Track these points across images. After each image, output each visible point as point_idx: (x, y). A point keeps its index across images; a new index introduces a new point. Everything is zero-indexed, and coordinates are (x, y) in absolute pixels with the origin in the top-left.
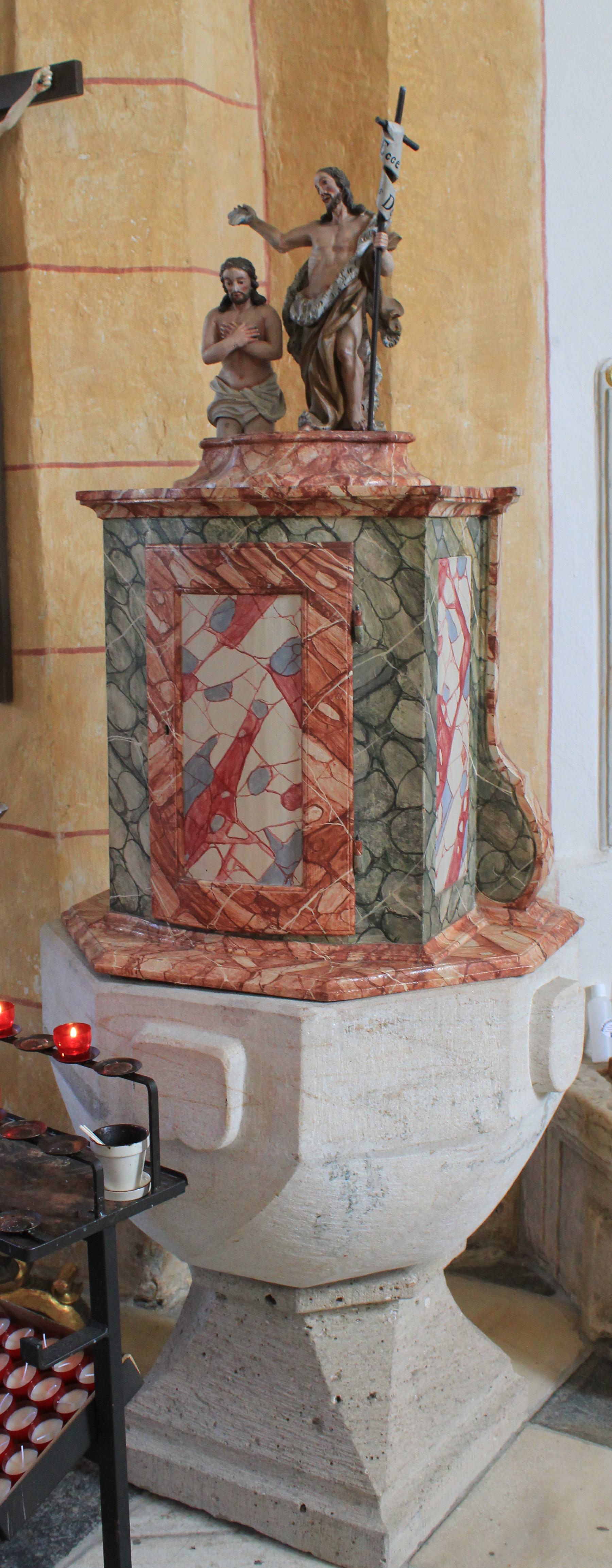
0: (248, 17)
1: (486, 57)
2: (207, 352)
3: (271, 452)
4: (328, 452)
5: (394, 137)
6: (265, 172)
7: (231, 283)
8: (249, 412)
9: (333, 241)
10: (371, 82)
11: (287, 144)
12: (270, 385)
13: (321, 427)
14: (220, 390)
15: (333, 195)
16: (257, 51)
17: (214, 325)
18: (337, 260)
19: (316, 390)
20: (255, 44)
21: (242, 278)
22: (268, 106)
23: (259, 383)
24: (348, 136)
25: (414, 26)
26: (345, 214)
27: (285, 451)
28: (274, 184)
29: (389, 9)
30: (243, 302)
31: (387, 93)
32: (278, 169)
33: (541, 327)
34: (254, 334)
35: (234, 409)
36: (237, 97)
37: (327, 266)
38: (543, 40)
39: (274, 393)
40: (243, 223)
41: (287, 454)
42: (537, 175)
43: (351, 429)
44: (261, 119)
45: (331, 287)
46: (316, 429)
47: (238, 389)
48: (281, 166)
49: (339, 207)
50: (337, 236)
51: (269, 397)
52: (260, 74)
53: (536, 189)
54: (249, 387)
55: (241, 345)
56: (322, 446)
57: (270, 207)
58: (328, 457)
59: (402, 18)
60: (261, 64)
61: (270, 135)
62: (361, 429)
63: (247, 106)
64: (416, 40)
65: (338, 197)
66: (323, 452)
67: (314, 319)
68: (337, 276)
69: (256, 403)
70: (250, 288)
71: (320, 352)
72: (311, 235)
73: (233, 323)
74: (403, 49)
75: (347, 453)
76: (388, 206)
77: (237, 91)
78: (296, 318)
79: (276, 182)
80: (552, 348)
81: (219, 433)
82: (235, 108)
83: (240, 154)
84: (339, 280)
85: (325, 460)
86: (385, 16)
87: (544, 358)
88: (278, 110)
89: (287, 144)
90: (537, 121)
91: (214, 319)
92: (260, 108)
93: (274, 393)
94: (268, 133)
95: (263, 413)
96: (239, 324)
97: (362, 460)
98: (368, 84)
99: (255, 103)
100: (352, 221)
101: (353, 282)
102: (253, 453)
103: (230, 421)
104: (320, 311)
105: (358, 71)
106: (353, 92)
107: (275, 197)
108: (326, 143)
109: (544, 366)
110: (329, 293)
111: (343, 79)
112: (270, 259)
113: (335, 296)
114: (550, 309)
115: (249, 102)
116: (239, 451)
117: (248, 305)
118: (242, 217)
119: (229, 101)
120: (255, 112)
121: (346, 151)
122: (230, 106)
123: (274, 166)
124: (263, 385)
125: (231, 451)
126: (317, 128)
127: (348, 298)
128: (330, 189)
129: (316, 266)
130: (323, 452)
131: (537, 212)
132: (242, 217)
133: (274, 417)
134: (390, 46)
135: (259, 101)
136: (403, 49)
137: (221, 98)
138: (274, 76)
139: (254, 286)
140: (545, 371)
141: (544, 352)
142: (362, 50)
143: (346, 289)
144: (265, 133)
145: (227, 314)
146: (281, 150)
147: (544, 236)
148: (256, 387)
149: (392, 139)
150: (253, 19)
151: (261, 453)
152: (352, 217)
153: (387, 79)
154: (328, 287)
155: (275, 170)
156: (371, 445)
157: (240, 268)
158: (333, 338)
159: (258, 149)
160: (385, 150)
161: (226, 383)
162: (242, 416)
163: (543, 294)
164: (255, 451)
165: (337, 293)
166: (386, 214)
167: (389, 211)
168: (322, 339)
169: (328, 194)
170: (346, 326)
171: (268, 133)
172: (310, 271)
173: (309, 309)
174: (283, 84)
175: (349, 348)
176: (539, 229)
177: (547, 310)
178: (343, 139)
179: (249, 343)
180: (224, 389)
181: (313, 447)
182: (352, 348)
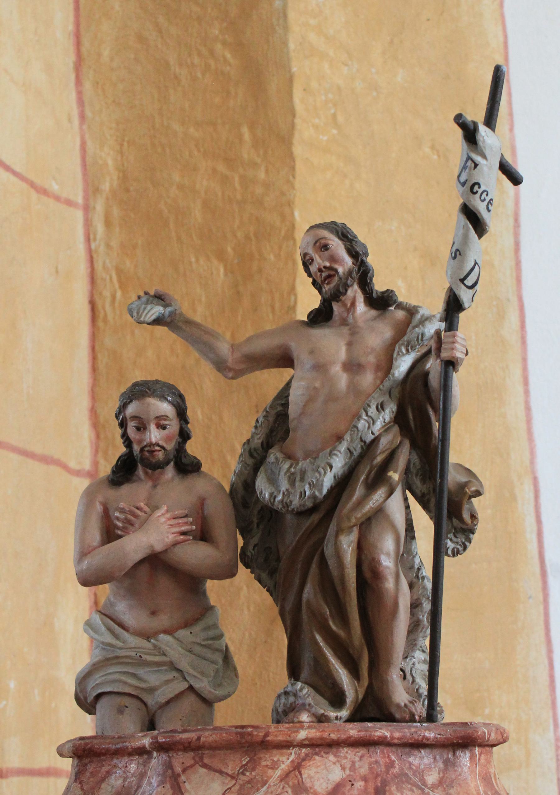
0: (73, 77)
1: (433, 148)
2: (85, 564)
3: (244, 769)
4: (364, 769)
5: (487, 153)
6: (93, 304)
7: (142, 427)
8: (168, 682)
9: (342, 354)
10: (267, 171)
11: (128, 263)
12: (208, 628)
13: (332, 714)
14: (108, 638)
15: (341, 270)
16: (85, 127)
17: (99, 508)
18: (353, 388)
19: (319, 638)
20: (82, 116)
21: (166, 417)
22: (99, 207)
23: (187, 625)
24: (229, 249)
25: (330, 96)
26: (361, 307)
27: (274, 766)
28: (105, 320)
29: (294, 69)
30: (160, 466)
31: (293, 188)
32: (114, 297)
33: (533, 547)
34: (184, 528)
35: (134, 676)
36: (55, 187)
37: (332, 398)
38: (511, 129)
39: (216, 644)
40: (158, 321)
41: (278, 773)
42: (513, 318)
43: (389, 718)
44: (88, 224)
45: (347, 437)
46: (321, 719)
47: (147, 636)
48: (119, 294)
49: (350, 292)
50: (349, 344)
51: (209, 654)
52: (89, 160)
53: (514, 339)
54: (168, 632)
55: (159, 547)
56: (349, 754)
57: (99, 356)
58: (365, 779)
59: (314, 84)
60: (90, 145)
61: (102, 249)
62: (412, 719)
63: (69, 203)
64: (334, 116)
65: (350, 273)
66: (353, 768)
67: (314, 497)
68: (359, 418)
69: (184, 664)
70: (177, 438)
71: (332, 562)
72: (293, 345)
73: (142, 505)
74: (316, 127)
75: (396, 770)
76: (469, 281)
77: (54, 178)
78: (273, 496)
79: (110, 317)
80: (552, 581)
81: (98, 725)
82: (51, 202)
83: (57, 272)
84: (362, 424)
85: (359, 784)
86: (290, 81)
87: (541, 596)
88: (116, 212)
89: (128, 263)
90: (509, 241)
91: (100, 498)
92: (87, 209)
93: (216, 644)
94: (98, 245)
95: (197, 685)
96: (156, 508)
97: (424, 783)
98: (262, 175)
99: (80, 200)
100: (374, 319)
101: (387, 429)
102: (203, 771)
103: (127, 701)
104: (328, 481)
105: (246, 156)
106: (237, 186)
107: (108, 341)
108: (193, 260)
109: (541, 607)
110: (343, 447)
111: (221, 168)
112: (98, 436)
113: (356, 454)
114: (544, 518)
115: (72, 197)
116: (169, 766)
117: (170, 471)
118: (157, 310)
119: (44, 192)
120: (79, 214)
121: (226, 274)
122: (45, 198)
123: (107, 294)
124: (197, 628)
125: (145, 764)
126: (179, 239)
127: (379, 459)
128: (333, 259)
129: (310, 400)
130: (353, 768)
131: (517, 372)
132: (157, 310)
133: (219, 692)
134: (298, 121)
135: (86, 198)
136: (316, 127)
137: (32, 185)
138: (110, 162)
139: (184, 435)
140: (542, 618)
141: (540, 584)
142: (252, 127)
143: (376, 440)
144: (93, 246)
145: (125, 489)
146: (119, 271)
147: (528, 408)
148: (182, 633)
149: (484, 157)
150: (78, 82)
151: (221, 772)
152: (374, 313)
153: (293, 169)
154: (339, 438)
155: (108, 300)
156: (437, 752)
157: (163, 398)
158: (354, 536)
159: (82, 268)
160: (470, 175)
161: (121, 625)
162: (152, 690)
163: (532, 495)
164: (205, 766)
165: (359, 450)
166: (464, 295)
167: (471, 292)
168: (337, 536)
169: (330, 268)
170: (380, 511)
171: (98, 245)
172: (293, 411)
173: (302, 479)
174: (124, 177)
175: (388, 554)
176: (521, 398)
177: (539, 521)
178: (221, 256)
179: (175, 544)
180: (116, 636)
181: (332, 757)
182: (392, 553)
